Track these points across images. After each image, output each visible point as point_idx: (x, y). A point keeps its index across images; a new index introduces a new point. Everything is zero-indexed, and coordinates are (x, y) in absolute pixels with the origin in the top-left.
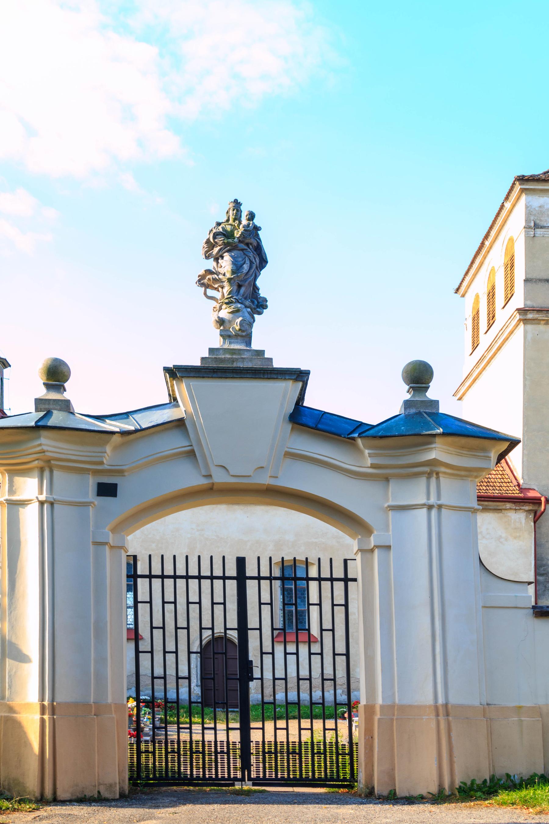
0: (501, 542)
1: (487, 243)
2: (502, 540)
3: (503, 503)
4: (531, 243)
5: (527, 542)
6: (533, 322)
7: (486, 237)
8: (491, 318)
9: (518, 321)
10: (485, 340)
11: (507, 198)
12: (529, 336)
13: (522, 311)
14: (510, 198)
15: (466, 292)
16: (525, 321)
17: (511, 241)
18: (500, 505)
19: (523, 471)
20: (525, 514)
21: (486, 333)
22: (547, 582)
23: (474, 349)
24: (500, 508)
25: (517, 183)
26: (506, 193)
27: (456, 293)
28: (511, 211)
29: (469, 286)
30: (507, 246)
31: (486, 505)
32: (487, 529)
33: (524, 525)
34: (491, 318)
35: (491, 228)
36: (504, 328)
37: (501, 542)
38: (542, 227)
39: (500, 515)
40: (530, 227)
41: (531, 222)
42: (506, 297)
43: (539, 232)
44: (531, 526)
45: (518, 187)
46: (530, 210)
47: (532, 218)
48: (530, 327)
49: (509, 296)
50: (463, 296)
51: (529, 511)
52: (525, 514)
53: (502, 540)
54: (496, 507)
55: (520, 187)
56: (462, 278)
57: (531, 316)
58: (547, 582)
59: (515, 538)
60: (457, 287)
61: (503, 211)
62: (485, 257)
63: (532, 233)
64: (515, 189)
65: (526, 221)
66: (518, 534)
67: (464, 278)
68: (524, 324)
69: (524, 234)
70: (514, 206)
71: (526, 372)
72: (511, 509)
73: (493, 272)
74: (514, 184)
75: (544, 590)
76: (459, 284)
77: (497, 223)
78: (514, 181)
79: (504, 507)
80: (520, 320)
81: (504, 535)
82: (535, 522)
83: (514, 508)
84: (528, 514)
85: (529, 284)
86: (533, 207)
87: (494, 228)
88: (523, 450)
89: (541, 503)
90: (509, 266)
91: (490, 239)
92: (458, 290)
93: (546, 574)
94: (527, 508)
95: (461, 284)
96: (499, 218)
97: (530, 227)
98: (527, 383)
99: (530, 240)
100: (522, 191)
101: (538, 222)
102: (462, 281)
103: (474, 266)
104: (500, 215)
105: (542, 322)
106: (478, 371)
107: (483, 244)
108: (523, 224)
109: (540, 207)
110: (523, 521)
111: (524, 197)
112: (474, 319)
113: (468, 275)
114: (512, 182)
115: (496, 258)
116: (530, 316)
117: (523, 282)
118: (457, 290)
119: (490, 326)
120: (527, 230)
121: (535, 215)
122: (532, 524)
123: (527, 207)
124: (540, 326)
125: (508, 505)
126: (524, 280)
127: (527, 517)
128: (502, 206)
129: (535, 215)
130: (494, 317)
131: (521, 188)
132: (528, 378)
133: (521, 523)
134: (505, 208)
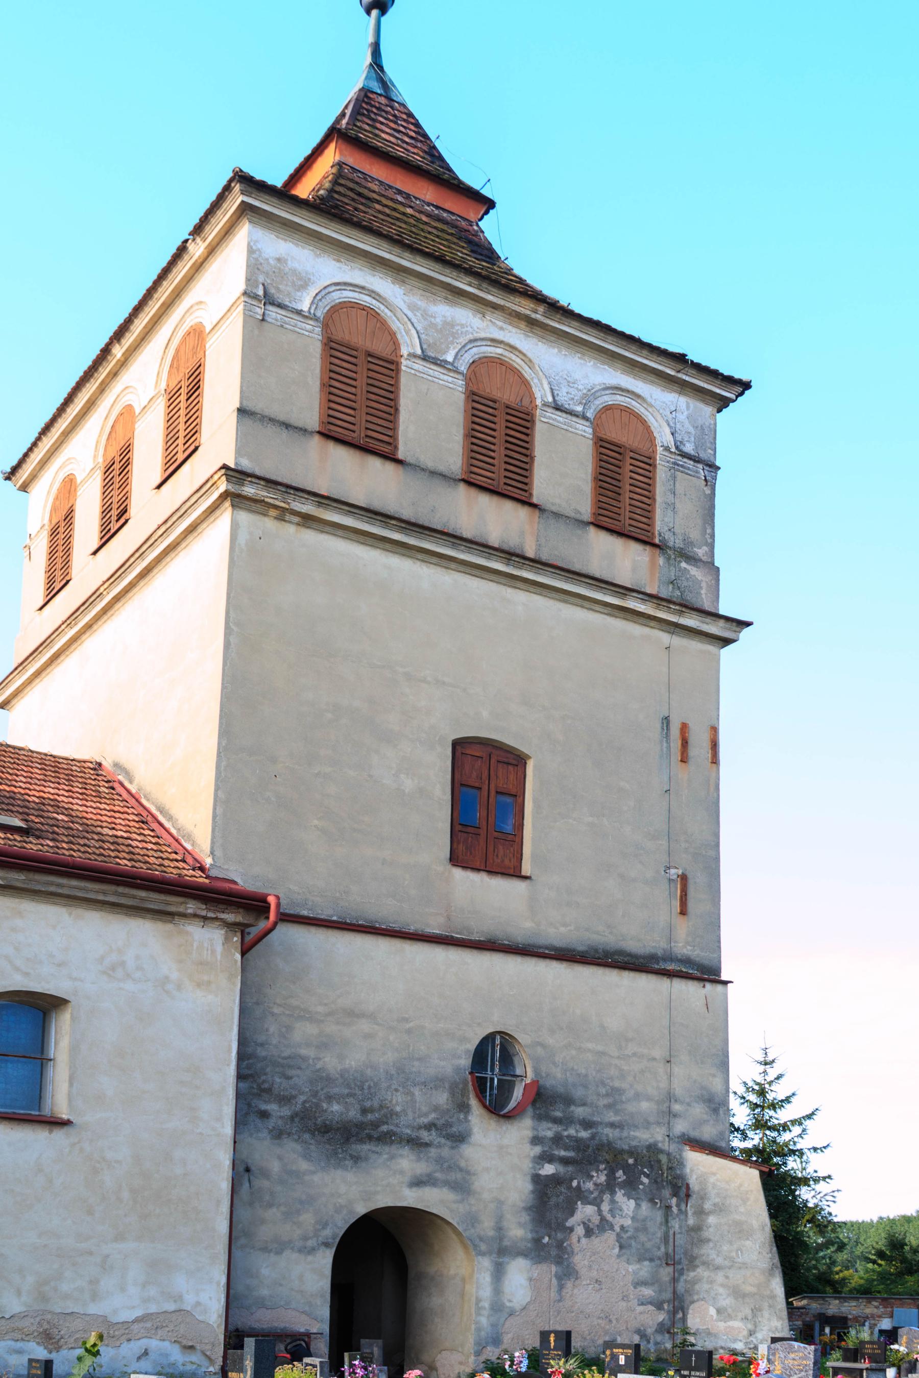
0: (167, 992)
1: (118, 352)
2: (170, 987)
3: (181, 899)
4: (256, 332)
5: (224, 999)
6: (254, 506)
7: (119, 335)
8: (115, 517)
9: (221, 496)
10: (89, 571)
11: (198, 230)
12: (242, 539)
13: (234, 474)
14: (207, 228)
15: (33, 477)
16: (235, 498)
17: (127, 416)
18: (175, 903)
19: (213, 837)
20: (223, 932)
21: (95, 553)
22: (254, 1094)
23: (52, 593)
24: (172, 909)
25: (237, 187)
26: (202, 214)
27: (8, 478)
28: (199, 267)
29: (43, 463)
30: (177, 351)
31: (142, 899)
32: (138, 957)
33: (219, 957)
34: (115, 517)
35: (137, 310)
36: (137, 555)
37: (167, 992)
38: (280, 306)
39: (169, 927)
40: (255, 297)
41: (257, 287)
42: (168, 463)
43: (274, 313)
44: (236, 961)
45: (237, 198)
46: (257, 259)
47: (261, 279)
48: (244, 517)
49: (181, 457)
50: (24, 488)
51: (231, 926)
52: (223, 932)
53: (170, 987)
54: (161, 907)
55: (241, 198)
56: (33, 440)
57: (253, 491)
58: (254, 1094)
59: (199, 985)
60: (14, 463)
61: (180, 264)
62: (102, 389)
63: (260, 311)
64: (225, 206)
65: (248, 280)
66: (206, 978)
67: (39, 439)
68: (233, 506)
69: (241, 307)
70: (211, 251)
71: (232, 615)
72: (195, 916)
73: (69, 486)
74: (227, 188)
75: (247, 1114)
76: (20, 455)
77: (156, 296)
78: (230, 181)
79: (181, 909)
80: (225, 495)
81: (174, 975)
82: (243, 954)
83: (204, 913)
84: (230, 934)
85: (248, 422)
86: (265, 255)
87: (147, 309)
88: (216, 790)
89: (269, 908)
90: (117, 466)
91: (129, 339)
92: (15, 470)
93: (251, 1076)
94: (230, 917)
95: (26, 455)
96: (165, 283)
97: (255, 297)
98: (232, 639)
99: (255, 326)
100: (245, 209)
101: (272, 291)
102: (30, 449)
103: (69, 410)
104: (170, 276)
105: (273, 512)
106: (71, 633)
107: (106, 351)
108: (241, 286)
109: (279, 260)
110: (219, 948)
111: (245, 231)
112: (54, 532)
113: (49, 434)
114: (224, 182)
115: (144, 380)
116: (249, 490)
117: (235, 413)
118: (10, 475)
119: (107, 536)
120: (250, 301)
121: (267, 274)
122: (238, 957)
123: (251, 251)
124: (266, 519)
125: (192, 907)
126: (239, 410)
127: (227, 939)
128: (182, 250)
129: (267, 274)
130: (125, 511)
131: (243, 202)
132: (235, 629)
133: (213, 952)
134: (186, 257)
